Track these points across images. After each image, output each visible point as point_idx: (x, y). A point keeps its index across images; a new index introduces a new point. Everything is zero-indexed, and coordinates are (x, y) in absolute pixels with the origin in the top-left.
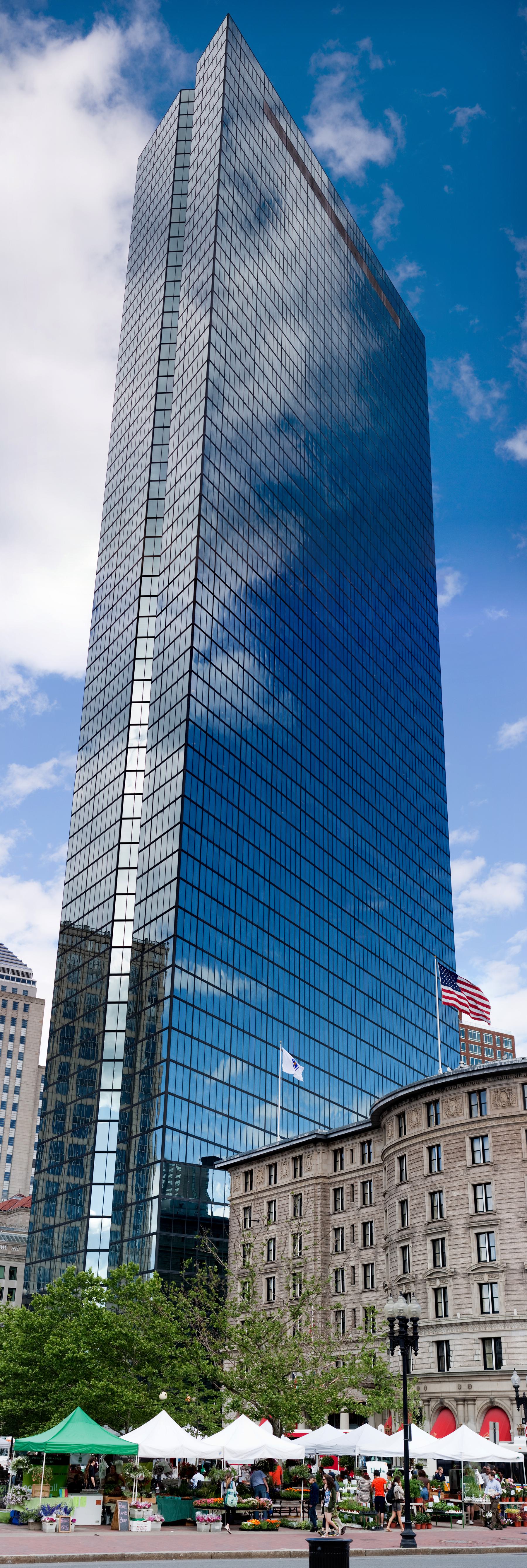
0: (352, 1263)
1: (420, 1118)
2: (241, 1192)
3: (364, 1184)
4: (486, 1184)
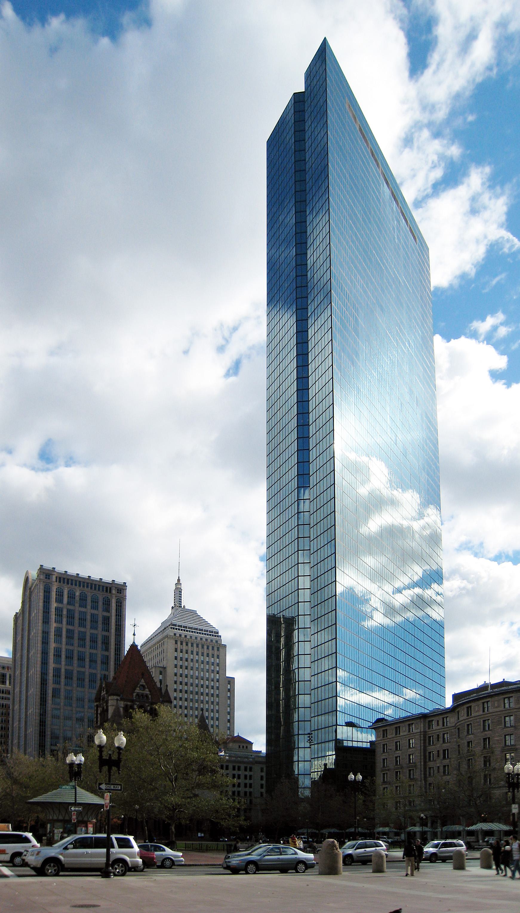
0: (438, 765)
2: (381, 738)
3: (468, 725)
4: (511, 735)
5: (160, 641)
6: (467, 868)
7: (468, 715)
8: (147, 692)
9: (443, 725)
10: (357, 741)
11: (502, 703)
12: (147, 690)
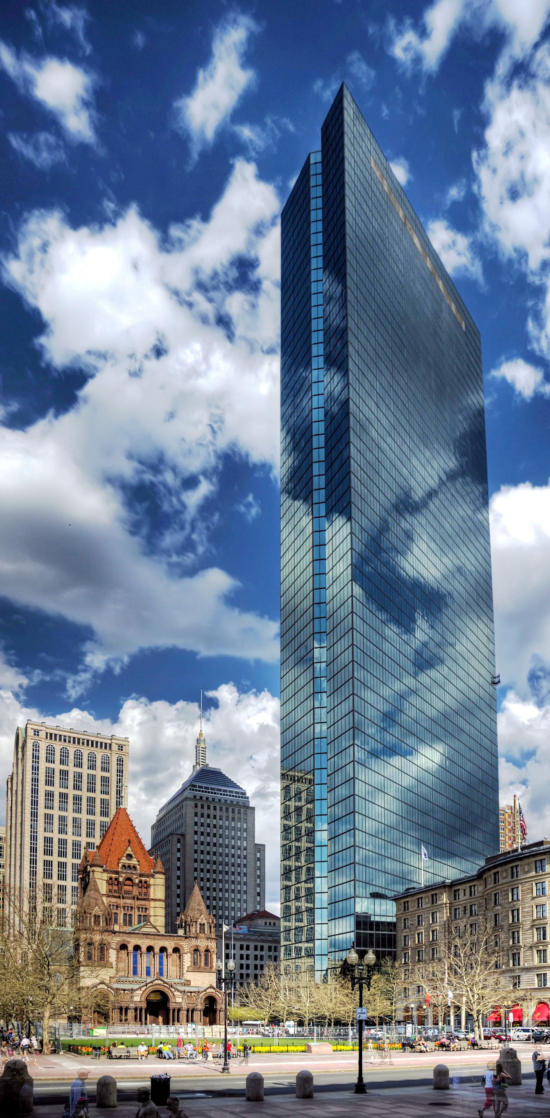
1: (507, 874)
2: (402, 911)
5: (178, 804)
7: (495, 883)
8: (134, 862)
9: (471, 895)
10: (380, 916)
12: (135, 859)
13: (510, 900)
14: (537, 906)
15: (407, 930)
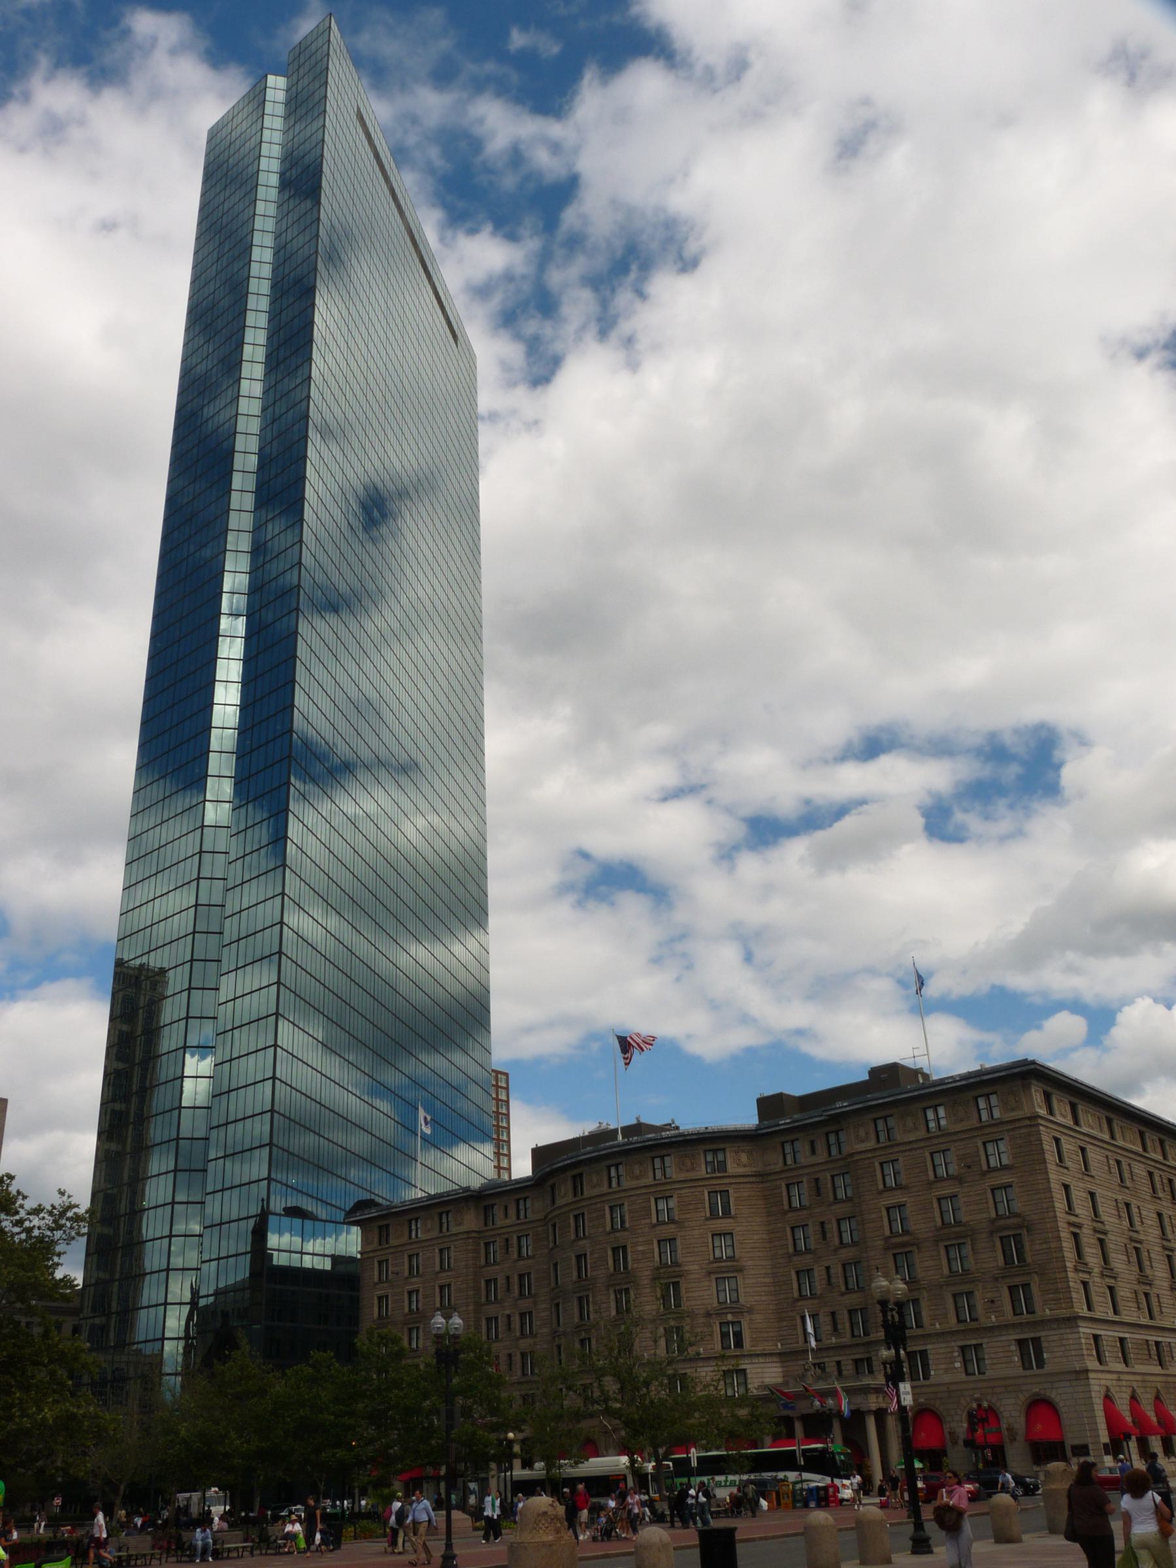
0: (507, 1312)
2: (375, 1245)
6: (935, 1550)
7: (575, 1195)
9: (518, 1218)
11: (605, 1179)
13: (608, 1228)
14: (659, 1242)
15: (385, 1285)
